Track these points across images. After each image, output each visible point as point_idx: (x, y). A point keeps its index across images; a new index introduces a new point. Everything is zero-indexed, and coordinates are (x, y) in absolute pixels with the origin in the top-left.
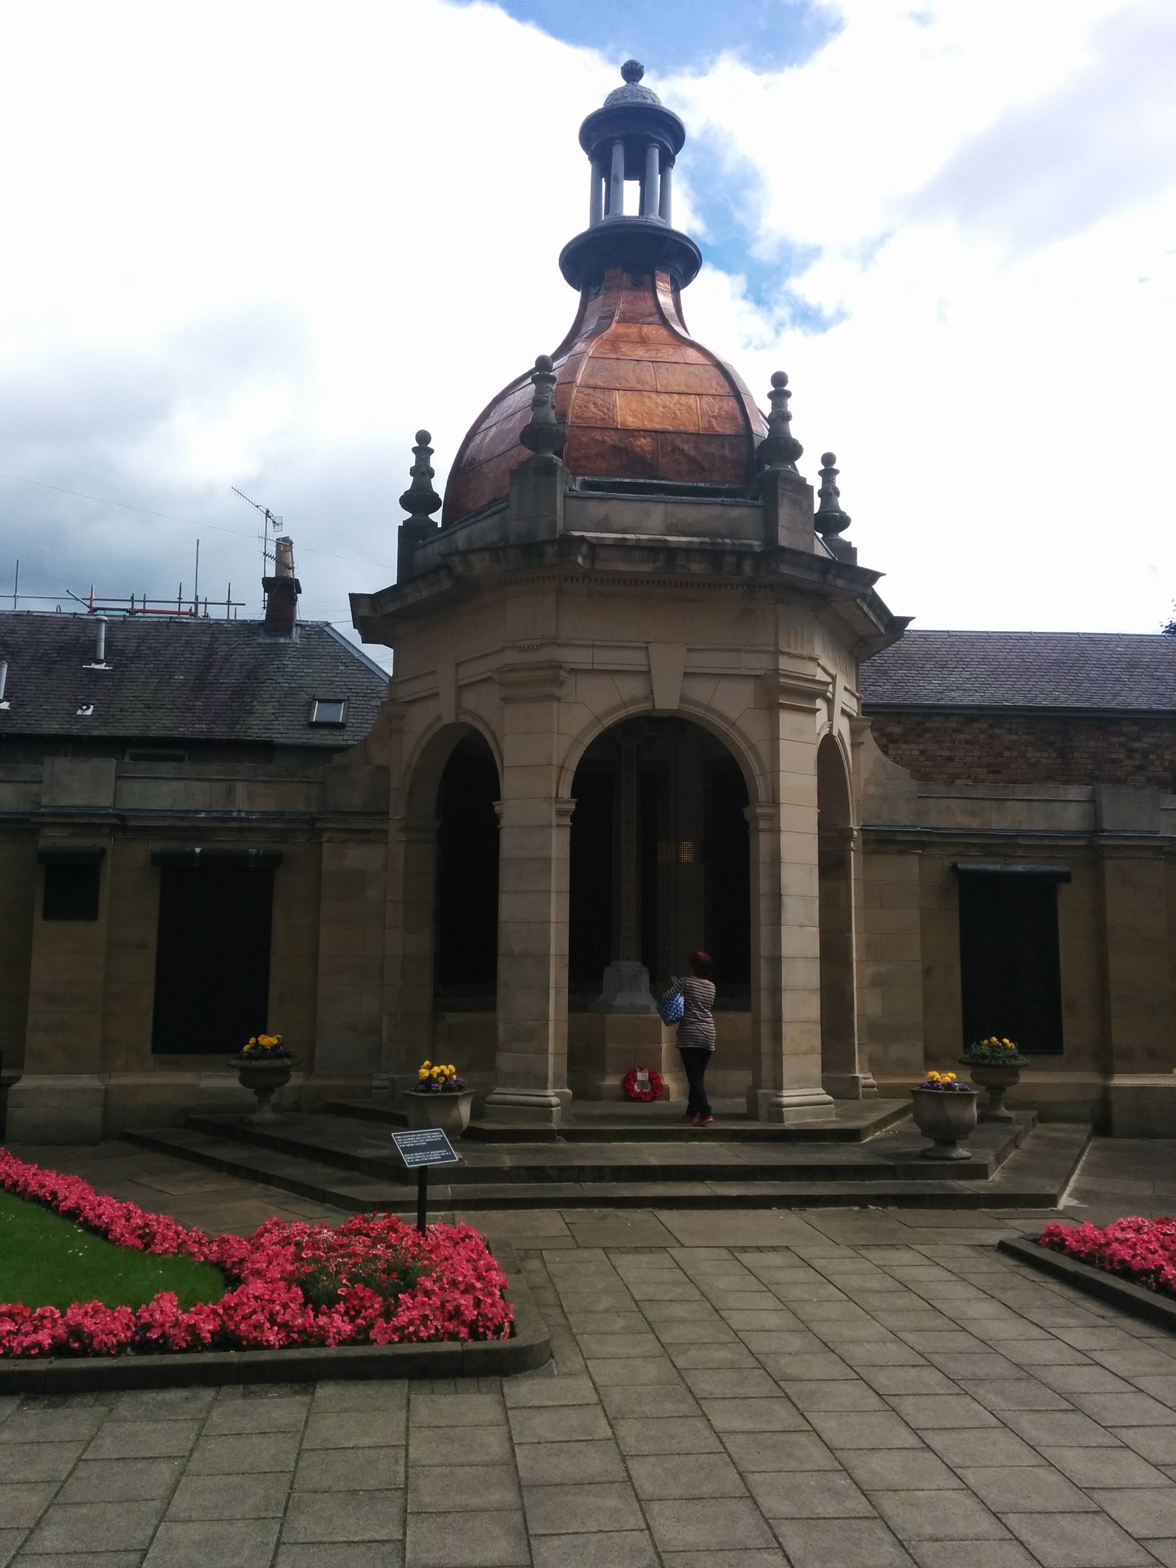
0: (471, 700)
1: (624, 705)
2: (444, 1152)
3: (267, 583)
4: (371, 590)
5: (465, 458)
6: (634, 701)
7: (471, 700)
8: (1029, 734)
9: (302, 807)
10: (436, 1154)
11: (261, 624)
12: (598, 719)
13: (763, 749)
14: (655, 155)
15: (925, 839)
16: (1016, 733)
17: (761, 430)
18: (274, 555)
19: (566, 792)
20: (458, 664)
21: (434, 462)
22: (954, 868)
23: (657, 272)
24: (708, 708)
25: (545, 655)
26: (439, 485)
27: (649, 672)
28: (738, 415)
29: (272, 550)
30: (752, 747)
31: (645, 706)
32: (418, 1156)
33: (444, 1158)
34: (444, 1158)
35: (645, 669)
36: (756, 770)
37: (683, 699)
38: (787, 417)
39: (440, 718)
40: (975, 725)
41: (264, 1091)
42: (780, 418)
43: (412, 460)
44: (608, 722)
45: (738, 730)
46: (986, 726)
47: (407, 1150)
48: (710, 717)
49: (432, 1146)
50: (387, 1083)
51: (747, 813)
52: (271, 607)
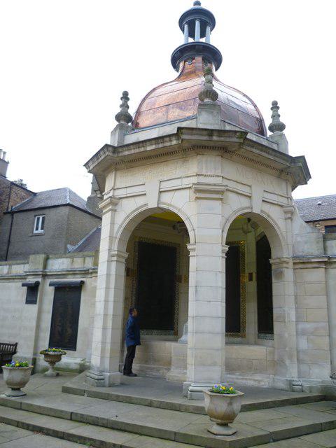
31: (249, 210)
39: (146, 205)
42: (276, 116)
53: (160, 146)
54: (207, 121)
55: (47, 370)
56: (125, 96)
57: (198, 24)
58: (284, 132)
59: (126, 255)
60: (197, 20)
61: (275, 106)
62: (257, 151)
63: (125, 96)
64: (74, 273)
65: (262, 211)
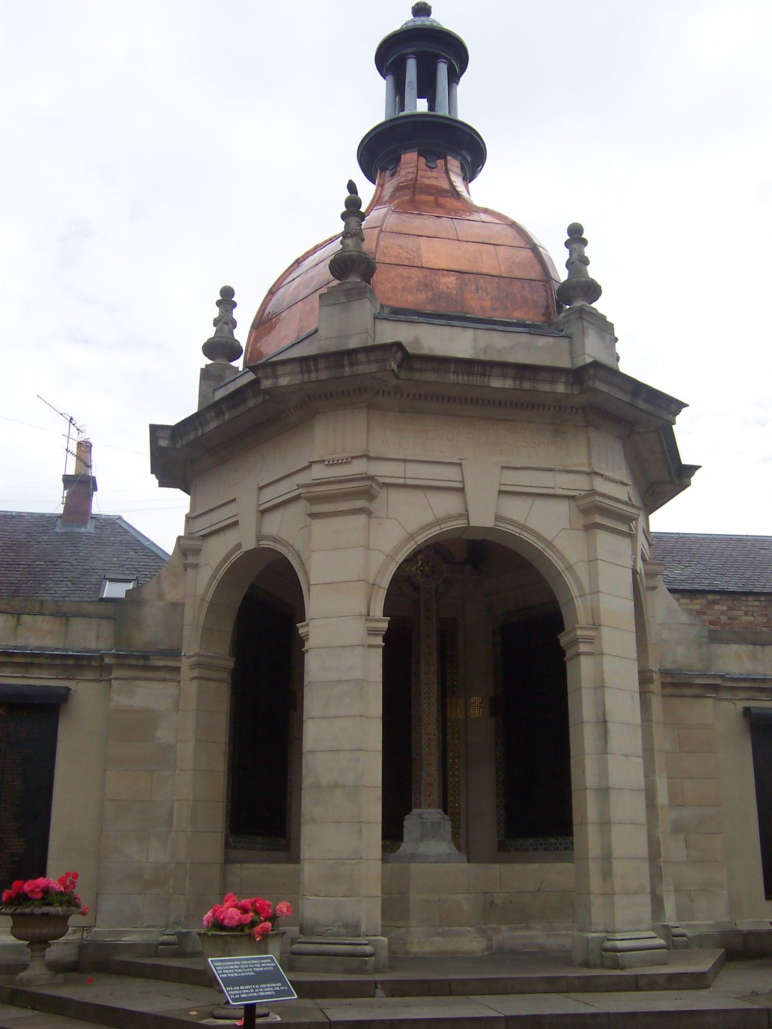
0: (274, 525)
1: (438, 522)
2: (278, 986)
3: (68, 481)
4: (172, 421)
5: (267, 312)
6: (448, 518)
7: (274, 525)
8: (762, 615)
9: (93, 645)
10: (268, 989)
11: (59, 517)
12: (412, 536)
13: (581, 570)
14: (442, 70)
15: (719, 682)
16: (752, 615)
17: (562, 274)
18: (75, 451)
19: (378, 610)
20: (260, 488)
21: (236, 314)
22: (747, 711)
23: (449, 158)
24: (524, 528)
25: (358, 468)
26: (242, 335)
27: (462, 490)
28: (535, 262)
29: (74, 448)
30: (569, 568)
31: (461, 523)
32: (245, 990)
33: (278, 994)
34: (278, 994)
35: (460, 485)
36: (575, 592)
37: (498, 518)
38: (586, 262)
39: (239, 546)
40: (716, 607)
41: (39, 943)
42: (577, 263)
43: (215, 312)
44: (421, 539)
45: (557, 551)
46: (725, 608)
47: (230, 982)
48: (525, 536)
49: (261, 978)
50: (173, 938)
51: (564, 639)
52: (69, 504)
53: (527, 385)
54: (361, 326)
55: (25, 967)
56: (227, 299)
57: (411, 66)
58: (599, 306)
59: (231, 664)
60: (422, 54)
61: (576, 237)
62: (433, 377)
63: (227, 299)
64: (30, 660)
65: (498, 518)
